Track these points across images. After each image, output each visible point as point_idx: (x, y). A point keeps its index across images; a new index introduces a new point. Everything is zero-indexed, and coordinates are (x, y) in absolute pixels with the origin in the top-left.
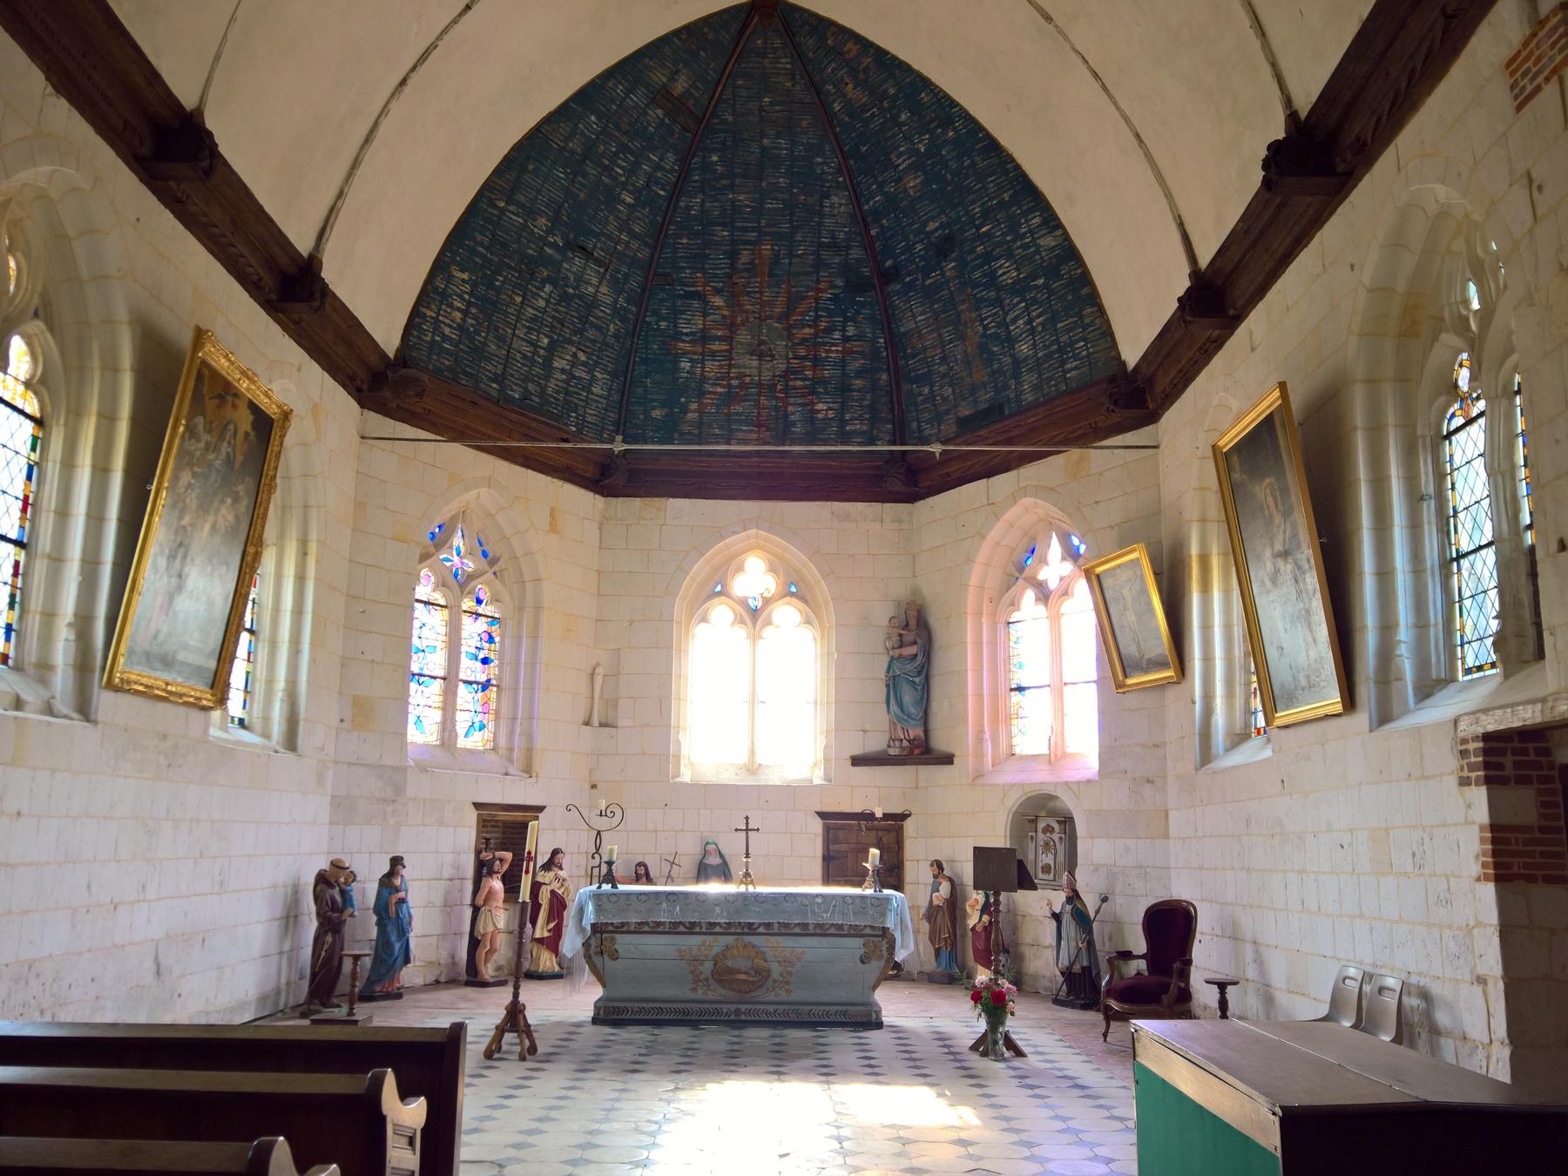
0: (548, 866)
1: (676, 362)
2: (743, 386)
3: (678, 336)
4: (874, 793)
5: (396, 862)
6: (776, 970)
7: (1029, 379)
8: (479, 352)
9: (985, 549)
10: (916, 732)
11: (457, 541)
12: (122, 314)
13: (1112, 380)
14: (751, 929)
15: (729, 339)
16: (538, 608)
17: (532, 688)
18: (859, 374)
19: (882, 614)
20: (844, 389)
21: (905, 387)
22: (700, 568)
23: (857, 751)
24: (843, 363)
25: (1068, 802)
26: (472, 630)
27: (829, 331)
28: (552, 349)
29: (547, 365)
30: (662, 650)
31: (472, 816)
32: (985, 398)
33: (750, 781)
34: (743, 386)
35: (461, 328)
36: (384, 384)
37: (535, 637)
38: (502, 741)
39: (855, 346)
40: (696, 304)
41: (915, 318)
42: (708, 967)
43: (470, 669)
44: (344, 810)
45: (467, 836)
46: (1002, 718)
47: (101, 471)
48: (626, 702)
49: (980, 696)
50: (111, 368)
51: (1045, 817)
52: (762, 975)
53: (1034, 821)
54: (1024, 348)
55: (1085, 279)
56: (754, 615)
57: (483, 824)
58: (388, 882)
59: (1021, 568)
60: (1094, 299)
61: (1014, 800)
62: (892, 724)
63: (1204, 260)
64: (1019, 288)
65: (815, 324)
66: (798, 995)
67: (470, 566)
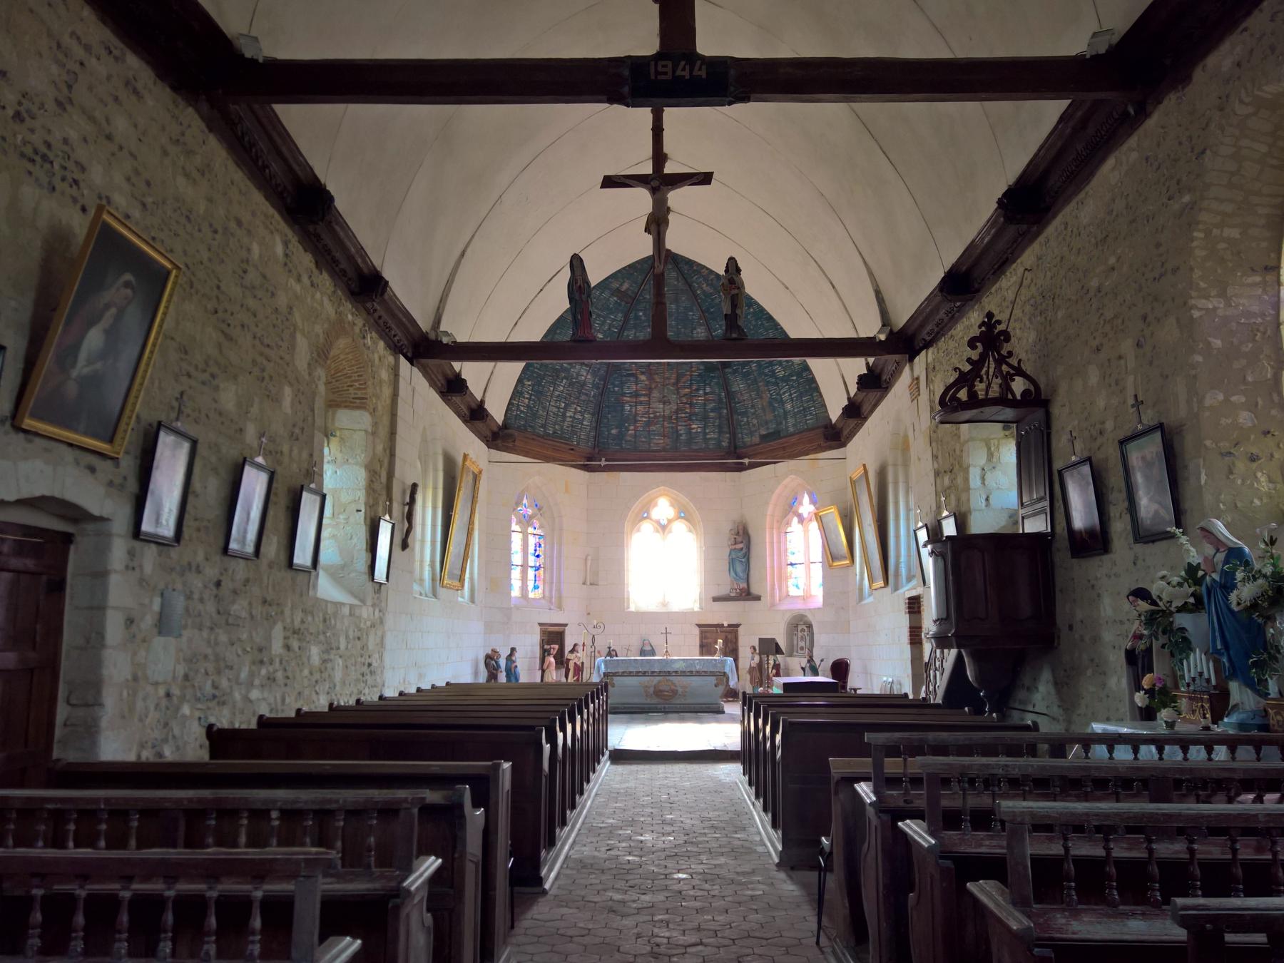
0: (572, 651)
1: (623, 407)
2: (655, 417)
3: (624, 394)
4: (724, 614)
5: (513, 650)
6: (680, 690)
7: (791, 421)
8: (535, 415)
9: (774, 497)
10: (744, 585)
11: (525, 501)
12: (440, 451)
13: (826, 427)
14: (669, 674)
15: (649, 395)
16: (561, 529)
17: (559, 569)
18: (712, 410)
19: (727, 527)
20: (705, 418)
21: (735, 417)
22: (636, 506)
23: (715, 594)
24: (705, 405)
25: (810, 618)
26: (532, 541)
27: (697, 390)
28: (565, 408)
29: (564, 415)
30: (619, 545)
31: (538, 629)
32: (772, 426)
33: (664, 610)
34: (655, 417)
35: (528, 406)
36: (498, 438)
37: (560, 545)
38: (547, 594)
39: (710, 397)
40: (632, 379)
41: (738, 385)
42: (652, 690)
43: (532, 561)
44: (489, 628)
45: (536, 638)
46: (783, 578)
47: (434, 508)
48: (603, 573)
49: (772, 567)
50: (436, 470)
51: (801, 626)
52: (675, 692)
53: (797, 626)
54: (788, 406)
55: (813, 380)
56: (663, 528)
57: (543, 633)
58: (510, 658)
59: (791, 506)
60: (817, 389)
61: (788, 617)
62: (732, 583)
63: (852, 395)
64: (786, 379)
65: (690, 386)
66: (689, 701)
67: (530, 512)
